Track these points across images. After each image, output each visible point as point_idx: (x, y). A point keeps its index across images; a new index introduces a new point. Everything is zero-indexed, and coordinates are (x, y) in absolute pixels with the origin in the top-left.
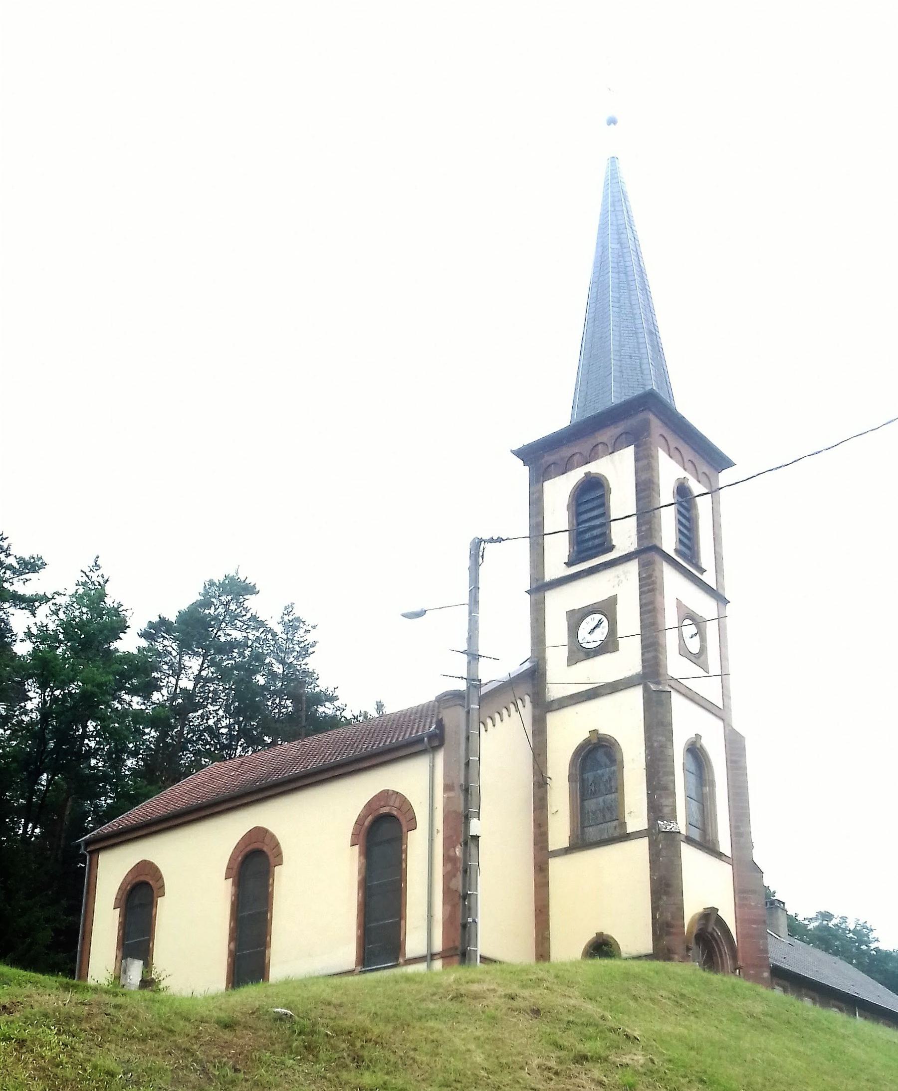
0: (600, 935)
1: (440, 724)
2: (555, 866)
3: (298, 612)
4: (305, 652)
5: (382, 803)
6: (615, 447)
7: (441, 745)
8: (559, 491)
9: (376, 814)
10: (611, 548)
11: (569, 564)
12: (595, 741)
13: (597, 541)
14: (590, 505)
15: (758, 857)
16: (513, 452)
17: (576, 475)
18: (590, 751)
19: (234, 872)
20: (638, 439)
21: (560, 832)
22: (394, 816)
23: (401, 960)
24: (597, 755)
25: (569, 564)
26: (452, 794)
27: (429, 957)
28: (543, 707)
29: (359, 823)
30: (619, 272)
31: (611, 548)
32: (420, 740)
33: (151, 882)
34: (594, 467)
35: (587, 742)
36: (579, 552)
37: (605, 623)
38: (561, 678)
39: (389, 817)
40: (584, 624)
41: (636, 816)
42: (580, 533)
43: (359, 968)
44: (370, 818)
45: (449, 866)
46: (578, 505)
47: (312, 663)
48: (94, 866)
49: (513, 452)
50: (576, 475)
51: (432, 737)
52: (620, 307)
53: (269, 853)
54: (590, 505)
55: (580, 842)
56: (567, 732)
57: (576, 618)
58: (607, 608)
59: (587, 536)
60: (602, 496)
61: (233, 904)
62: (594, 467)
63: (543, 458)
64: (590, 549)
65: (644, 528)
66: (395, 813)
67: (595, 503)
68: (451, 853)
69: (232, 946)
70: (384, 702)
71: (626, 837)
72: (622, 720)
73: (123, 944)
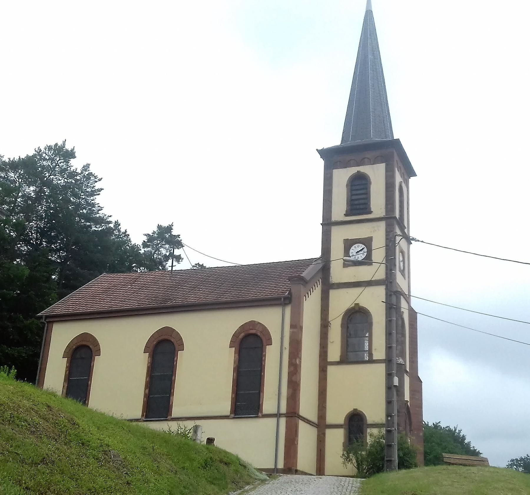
0: (355, 410)
1: (290, 293)
2: (331, 370)
3: (92, 169)
4: (96, 192)
5: (251, 328)
6: (374, 161)
7: (290, 303)
8: (342, 176)
9: (247, 333)
10: (370, 212)
11: (346, 215)
12: (357, 309)
13: (361, 207)
14: (358, 187)
15: (420, 375)
16: (317, 150)
17: (353, 171)
18: (353, 313)
19: (151, 348)
20: (387, 160)
21: (334, 352)
22: (259, 337)
23: (260, 415)
24: (357, 317)
25: (346, 215)
26: (295, 330)
27: (278, 416)
28: (328, 286)
29: (235, 335)
30: (373, 71)
31: (370, 212)
32: (279, 299)
33: (91, 347)
34: (363, 169)
35: (353, 308)
36: (351, 210)
37: (365, 250)
38: (339, 273)
39: (255, 335)
40: (353, 248)
41: (380, 353)
42: (352, 200)
43: (233, 415)
44: (242, 335)
45: (292, 369)
46: (352, 186)
47: (98, 200)
48: (50, 331)
49: (317, 150)
50: (353, 171)
51: (285, 298)
52: (374, 89)
53: (175, 343)
54: (358, 187)
55: (344, 360)
56: (341, 302)
57: (348, 244)
58: (367, 242)
59: (356, 202)
60: (366, 184)
61: (148, 367)
62: (363, 169)
63: (332, 158)
64: (357, 209)
65: (389, 206)
66: (259, 334)
67: (362, 187)
68: (294, 361)
69: (147, 391)
70: (120, 222)
71: (371, 361)
72: (374, 300)
73: (69, 379)
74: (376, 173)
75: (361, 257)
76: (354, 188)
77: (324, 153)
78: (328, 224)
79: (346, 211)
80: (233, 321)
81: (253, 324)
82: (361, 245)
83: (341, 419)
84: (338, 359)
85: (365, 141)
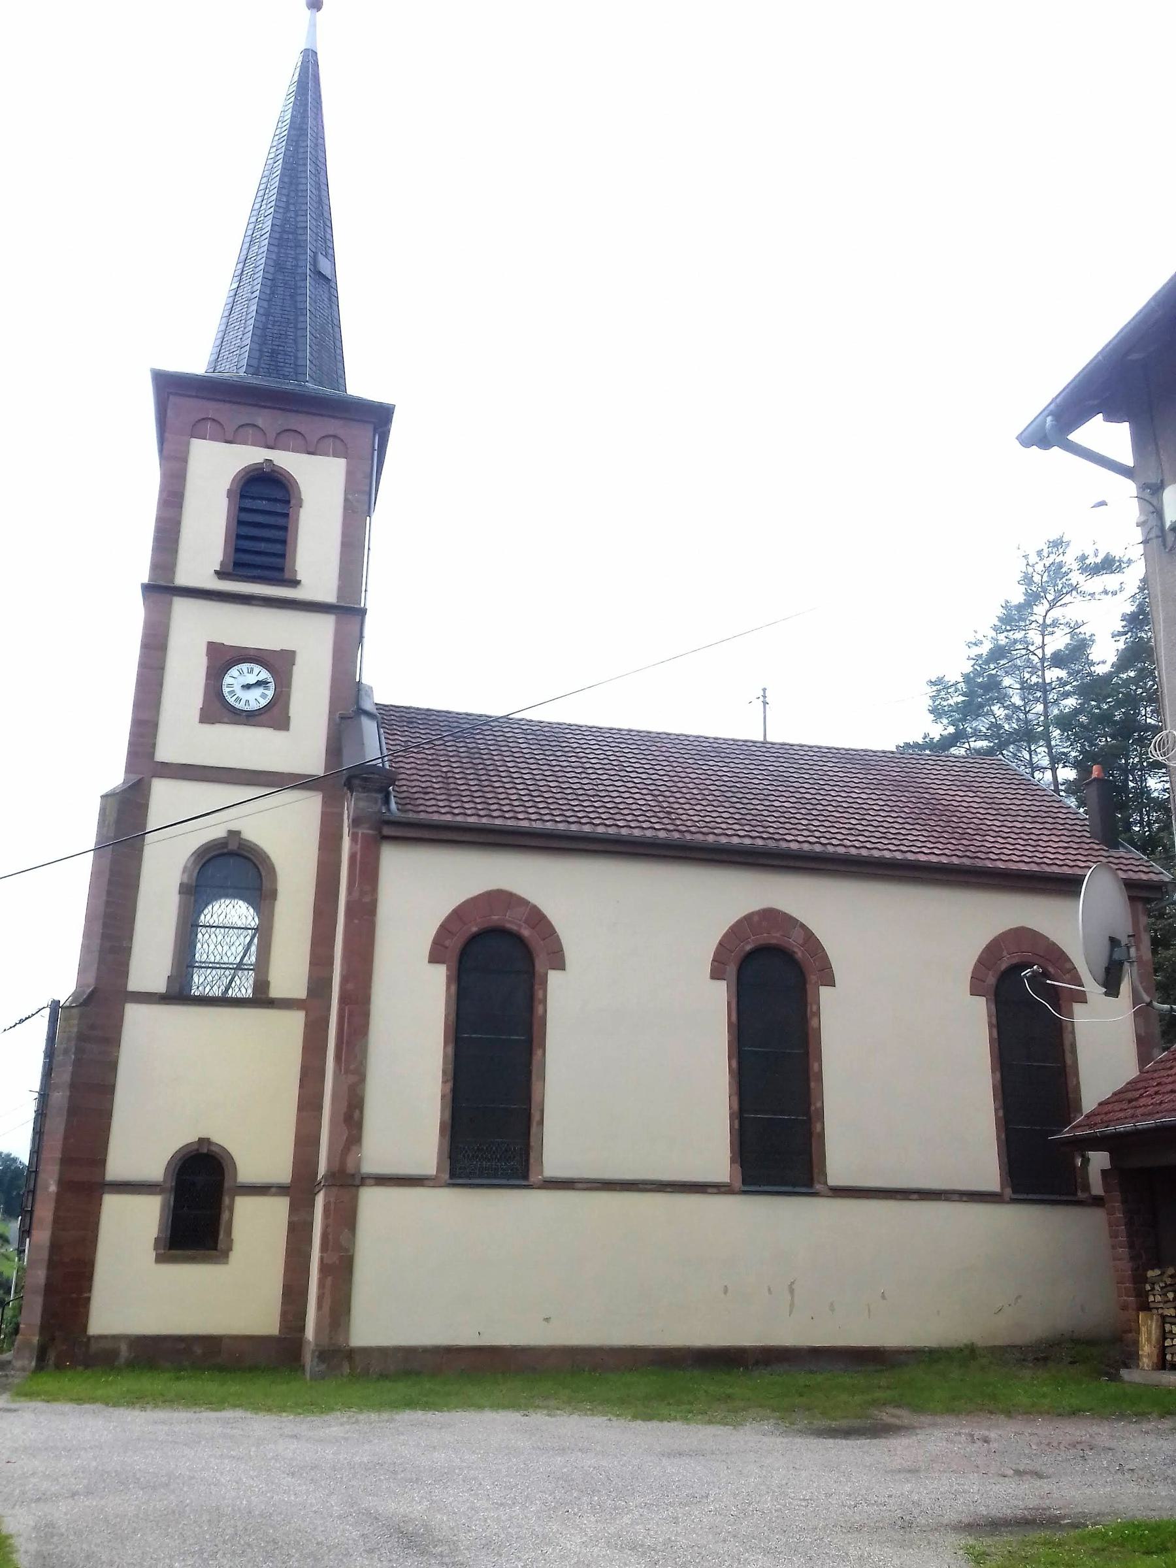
0: (203, 1141)
8: (217, 465)
12: (233, 846)
17: (251, 455)
25: (221, 574)
29: (445, 930)
31: (295, 583)
34: (288, 461)
36: (237, 564)
40: (234, 671)
46: (242, 496)
50: (251, 455)
62: (288, 461)
63: (188, 405)
74: (318, 479)
75: (256, 699)
76: (248, 504)
77: (172, 389)
78: (162, 590)
79: (222, 564)
80: (725, 900)
81: (771, 917)
82: (257, 668)
83: (155, 1168)
84: (159, 985)
85: (290, 385)
